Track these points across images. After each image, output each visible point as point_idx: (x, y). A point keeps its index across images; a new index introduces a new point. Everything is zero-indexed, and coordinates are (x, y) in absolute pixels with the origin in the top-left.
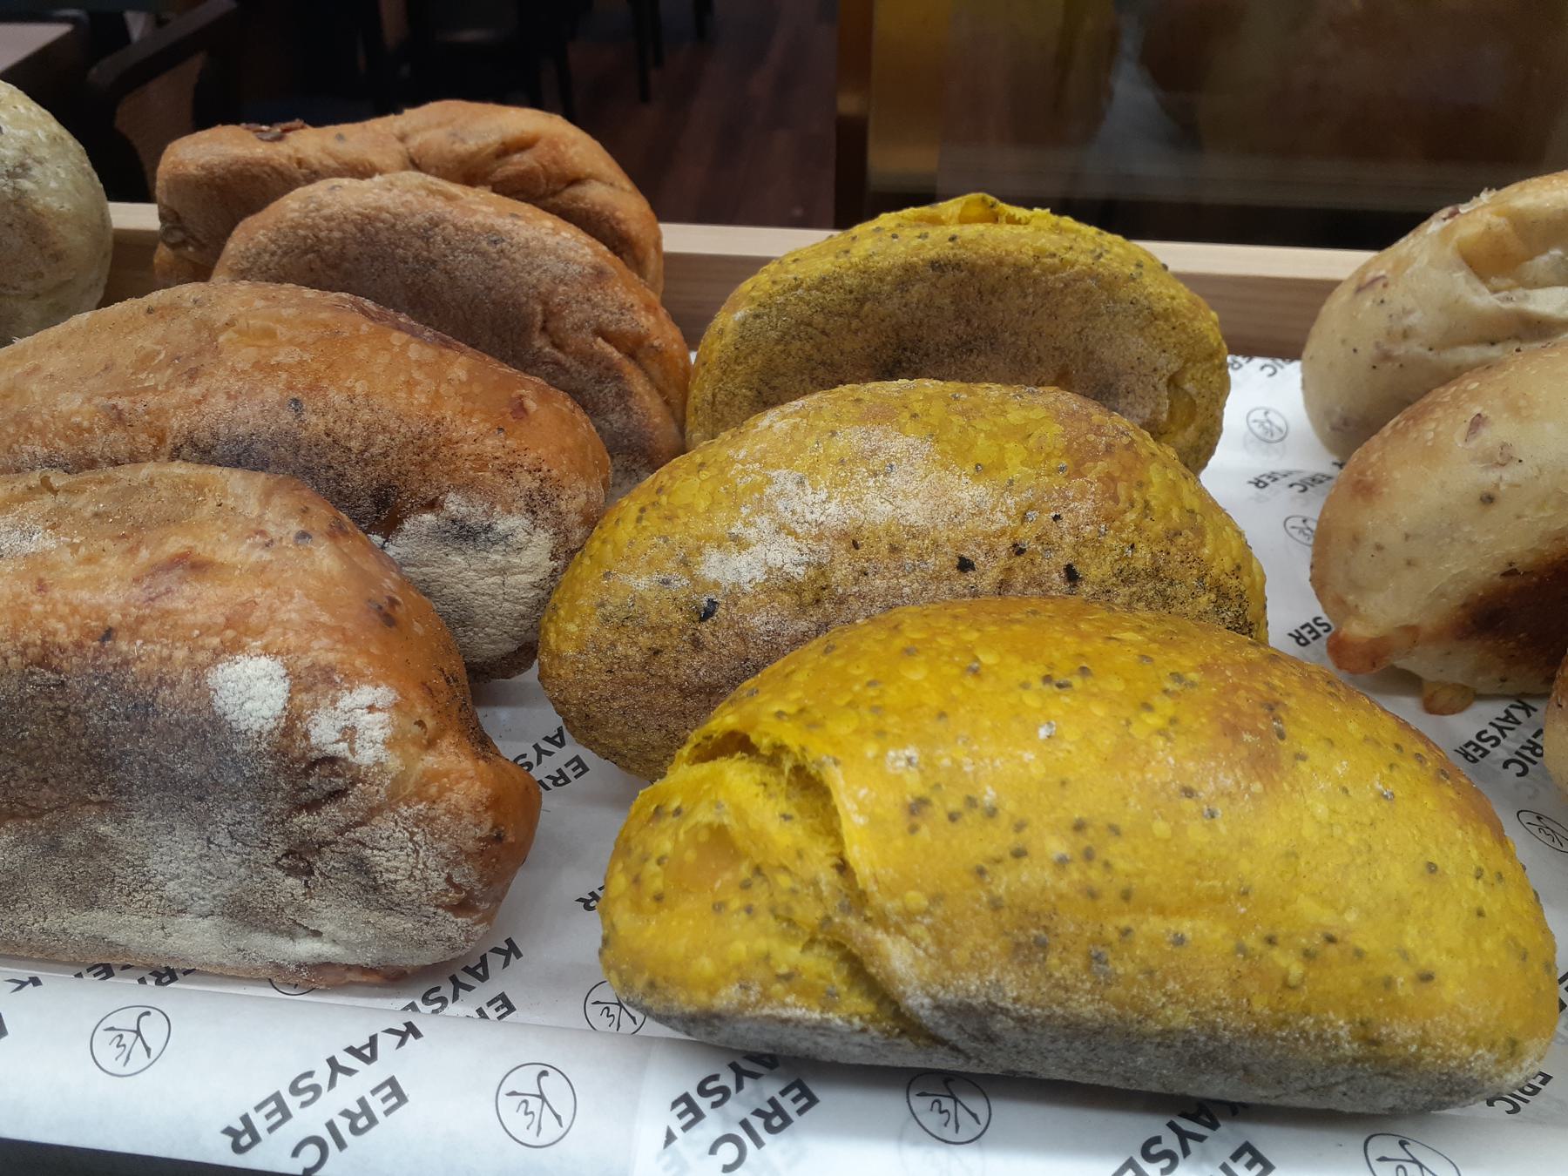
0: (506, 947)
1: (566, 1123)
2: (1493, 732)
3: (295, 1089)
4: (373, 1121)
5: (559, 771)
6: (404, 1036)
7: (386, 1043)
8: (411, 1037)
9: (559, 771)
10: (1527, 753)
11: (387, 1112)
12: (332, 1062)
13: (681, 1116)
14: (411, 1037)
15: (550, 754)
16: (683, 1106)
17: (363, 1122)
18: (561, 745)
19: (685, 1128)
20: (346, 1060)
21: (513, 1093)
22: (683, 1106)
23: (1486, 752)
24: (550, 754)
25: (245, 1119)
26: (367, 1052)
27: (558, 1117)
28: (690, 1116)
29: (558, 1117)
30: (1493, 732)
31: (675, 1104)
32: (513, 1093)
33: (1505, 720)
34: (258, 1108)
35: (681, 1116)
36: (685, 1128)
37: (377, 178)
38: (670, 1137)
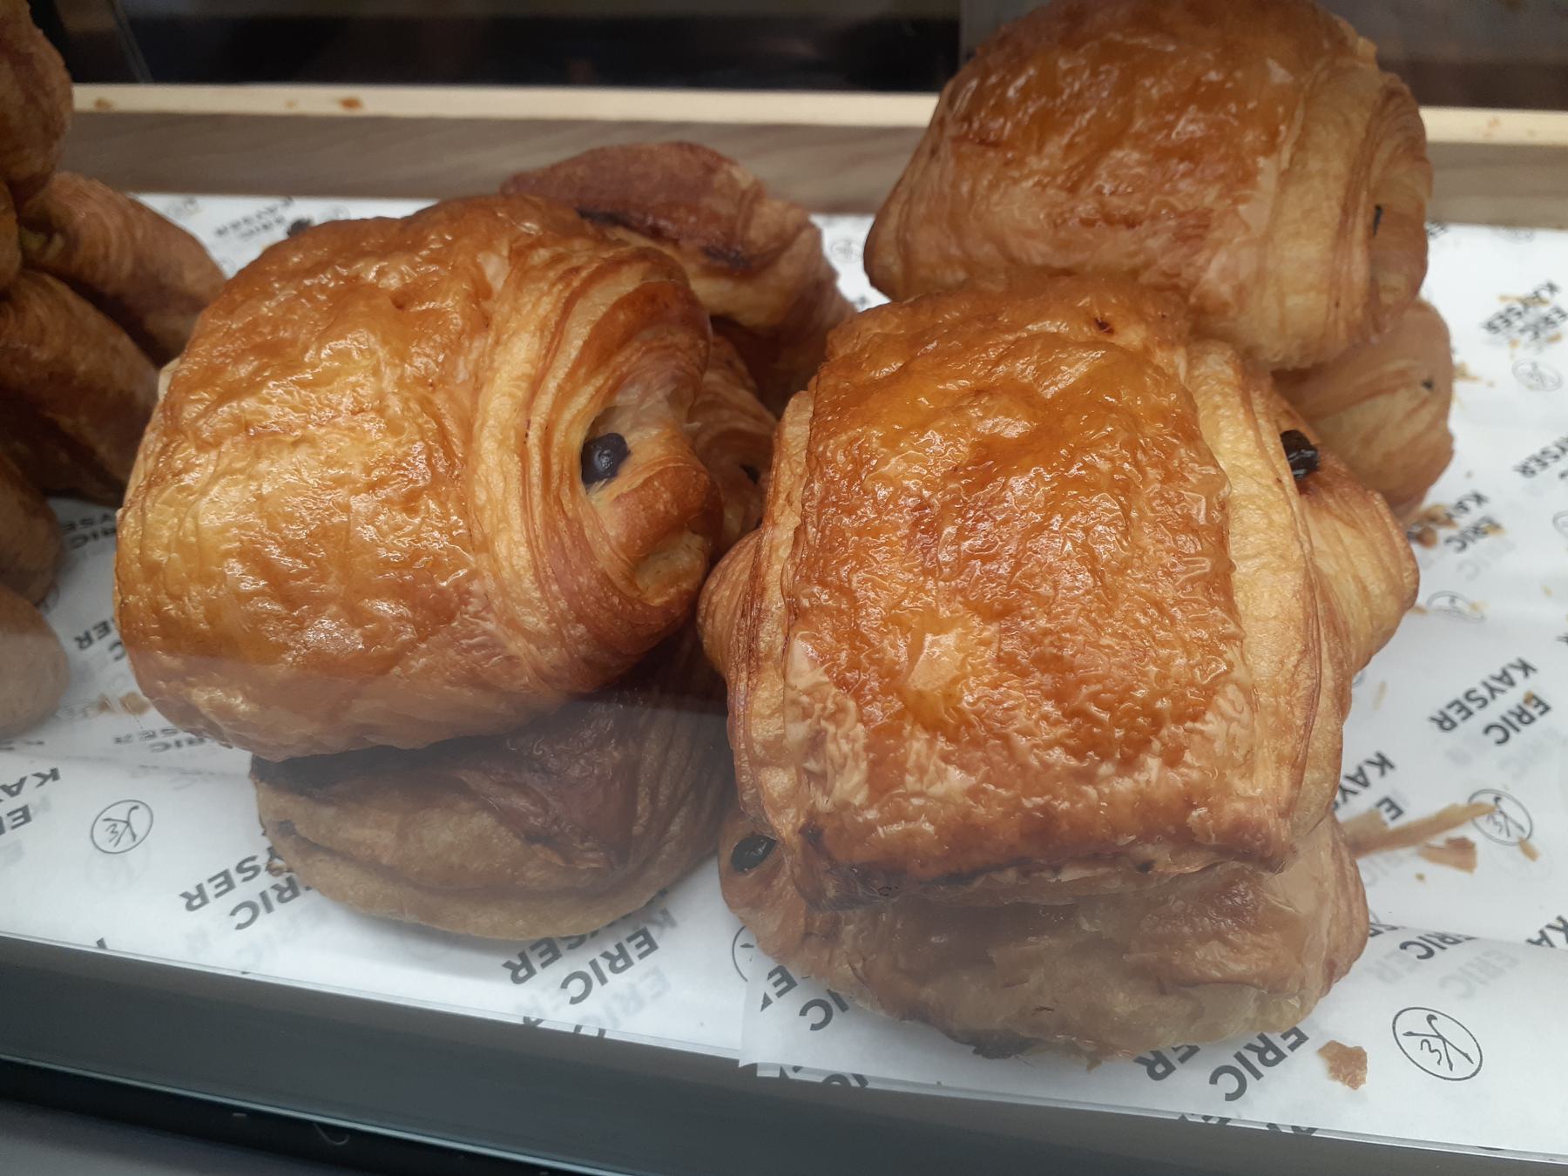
1: (1475, 1058)
2: (1484, 692)
3: (240, 869)
4: (205, 901)
6: (45, 778)
7: (1372, 773)
10: (1513, 719)
11: (217, 896)
13: (776, 984)
15: (1355, 793)
16: (778, 976)
17: (197, 902)
19: (779, 994)
22: (778, 976)
23: (1470, 713)
25: (199, 887)
27: (1466, 1055)
28: (784, 985)
29: (1466, 1055)
30: (1484, 692)
31: (771, 975)
33: (1500, 679)
34: (211, 880)
35: (776, 984)
36: (779, 994)
37: (1327, 566)
38: (767, 1002)
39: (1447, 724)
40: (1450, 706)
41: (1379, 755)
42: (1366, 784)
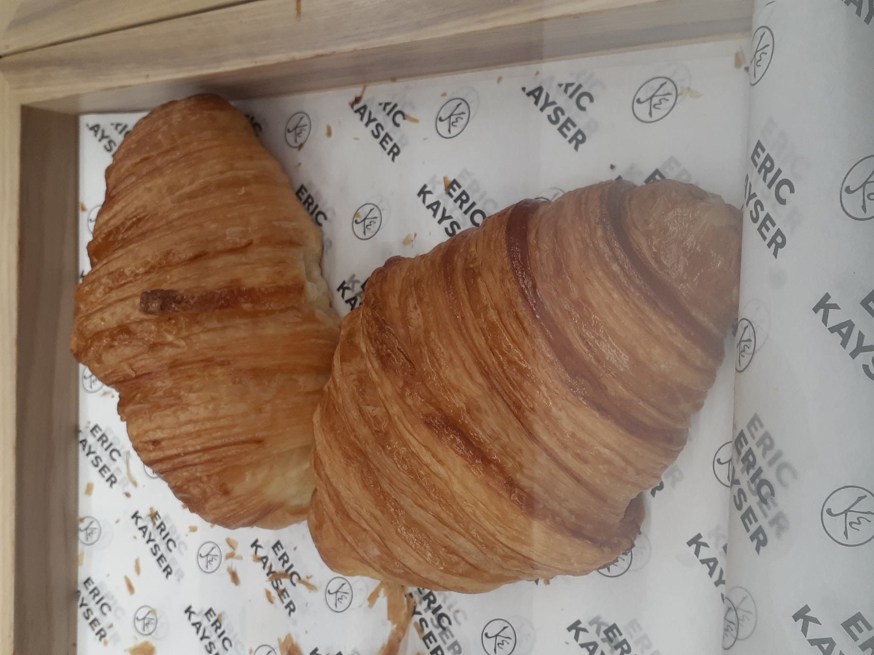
0: (822, 311)
3: (155, 554)
5: (389, 153)
7: (835, 317)
8: (427, 189)
9: (389, 153)
12: (854, 355)
14: (427, 189)
15: (861, 336)
17: (625, 647)
18: (850, 325)
20: (852, 344)
21: (846, 533)
24: (861, 336)
26: (711, 564)
32: (846, 533)
39: (779, 240)
40: (565, 136)
41: (816, 309)
42: (850, 325)
